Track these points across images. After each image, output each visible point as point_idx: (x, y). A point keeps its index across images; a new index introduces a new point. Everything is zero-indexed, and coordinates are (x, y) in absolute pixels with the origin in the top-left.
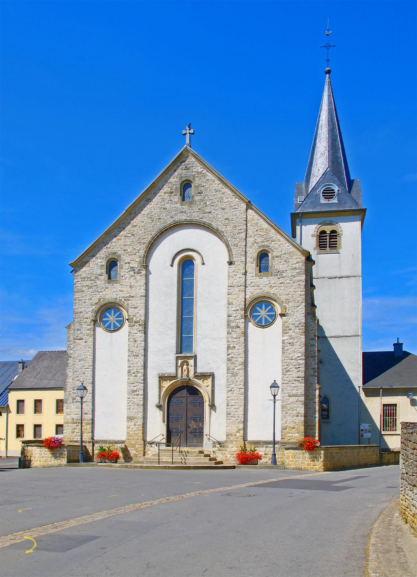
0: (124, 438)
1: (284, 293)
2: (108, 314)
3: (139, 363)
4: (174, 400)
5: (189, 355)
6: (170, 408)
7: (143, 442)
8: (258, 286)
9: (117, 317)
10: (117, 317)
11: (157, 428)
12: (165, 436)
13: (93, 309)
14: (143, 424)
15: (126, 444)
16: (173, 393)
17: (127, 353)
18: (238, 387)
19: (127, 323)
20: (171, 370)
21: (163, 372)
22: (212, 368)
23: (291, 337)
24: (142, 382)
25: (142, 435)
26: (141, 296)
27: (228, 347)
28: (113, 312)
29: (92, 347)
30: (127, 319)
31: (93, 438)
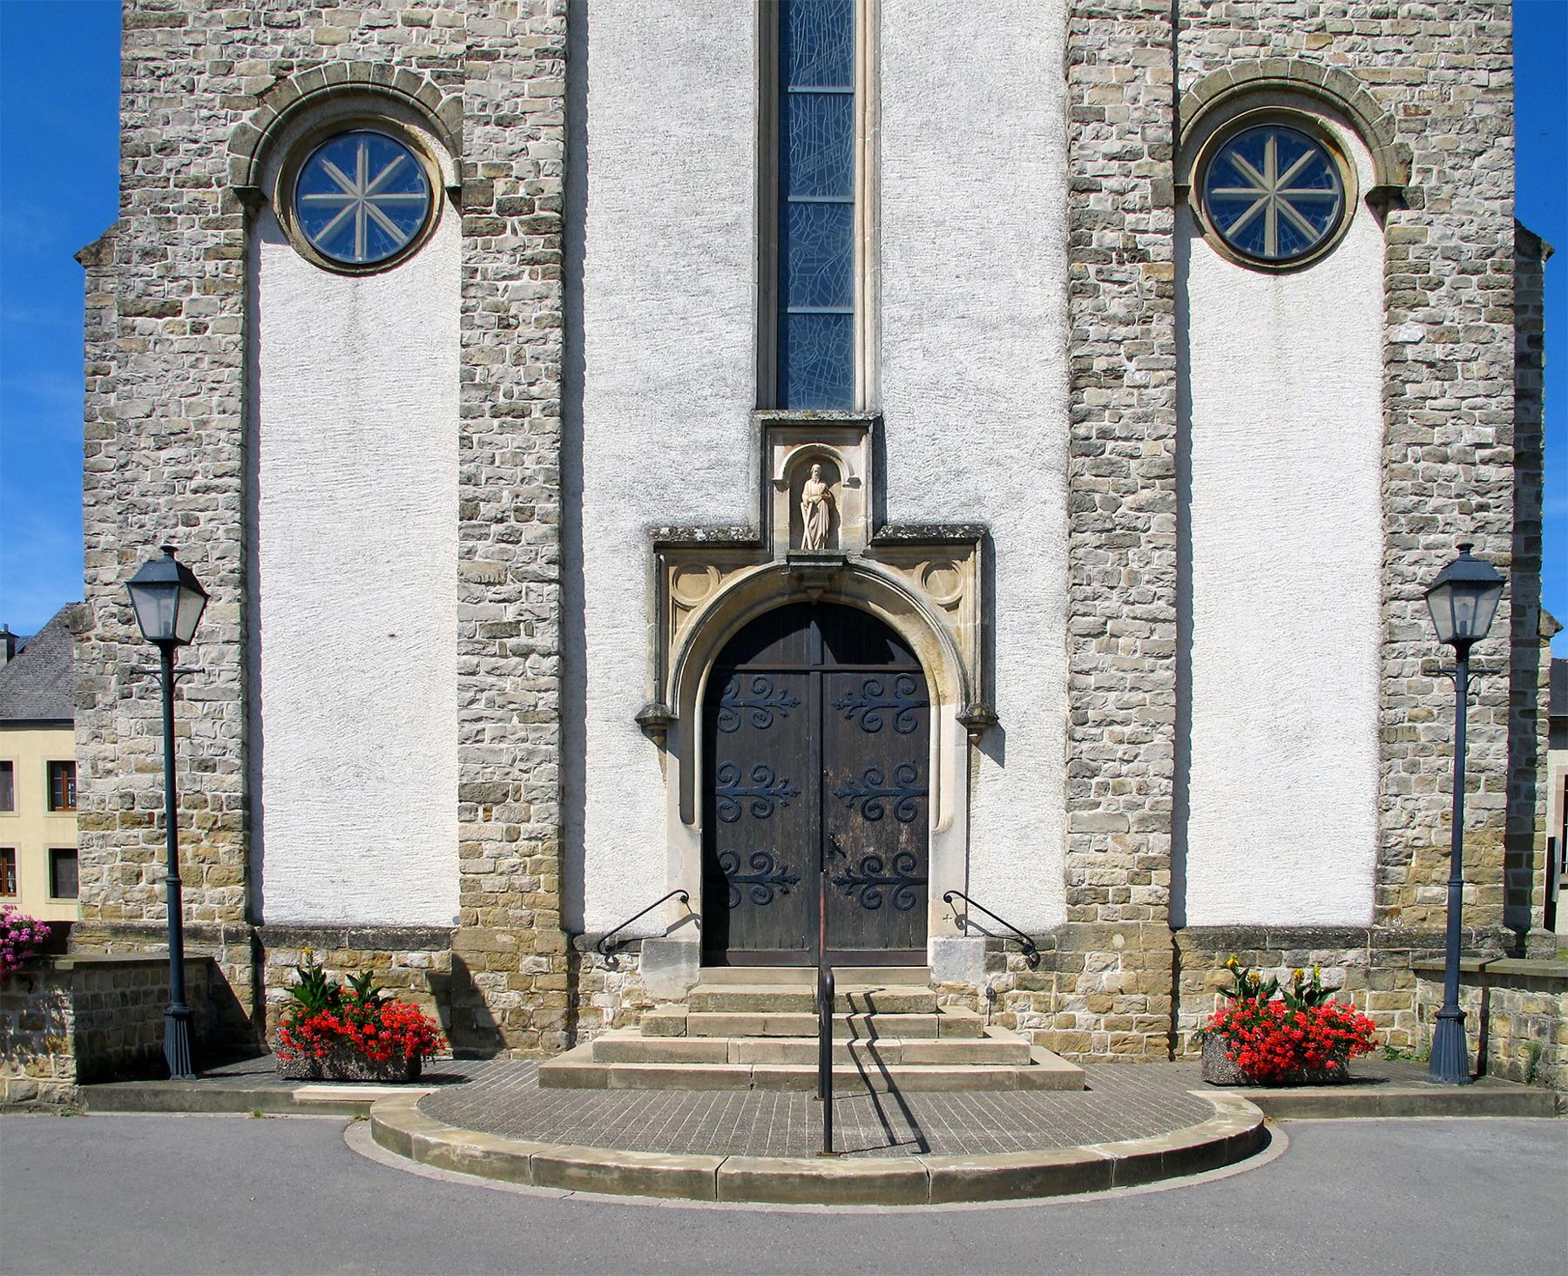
0: (443, 911)
1: (1396, 71)
2: (332, 169)
3: (529, 460)
4: (741, 687)
5: (836, 415)
6: (721, 741)
7: (561, 941)
8: (1248, 23)
9: (392, 186)
10: (392, 186)
11: (643, 853)
12: (696, 906)
13: (243, 130)
14: (562, 830)
15: (461, 947)
16: (733, 647)
17: (455, 399)
18: (1139, 609)
19: (450, 223)
20: (731, 507)
21: (682, 517)
22: (979, 501)
23: (1438, 330)
24: (554, 572)
25: (554, 899)
26: (543, 53)
27: (1079, 377)
28: (362, 156)
29: (237, 357)
30: (455, 194)
31: (252, 913)
